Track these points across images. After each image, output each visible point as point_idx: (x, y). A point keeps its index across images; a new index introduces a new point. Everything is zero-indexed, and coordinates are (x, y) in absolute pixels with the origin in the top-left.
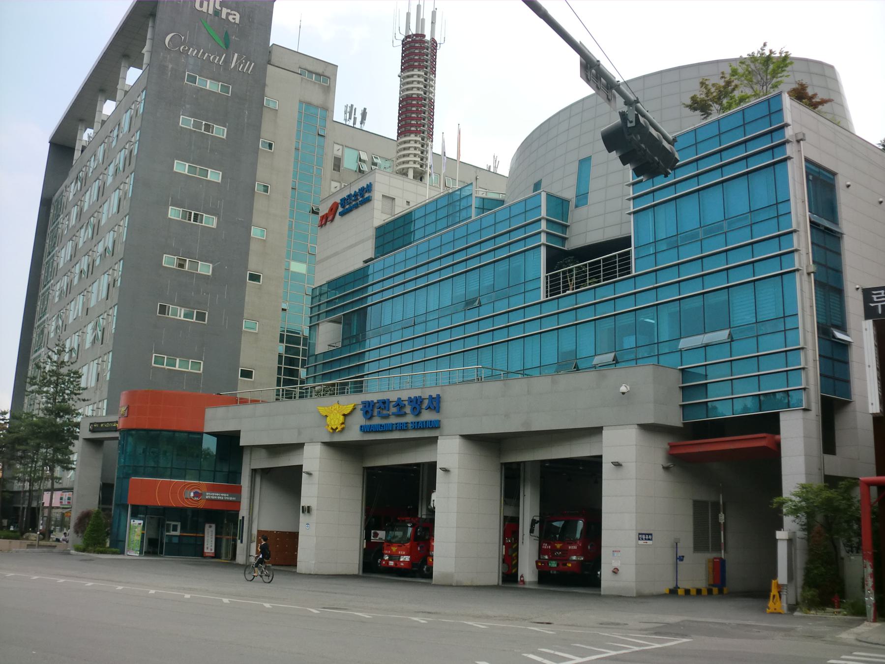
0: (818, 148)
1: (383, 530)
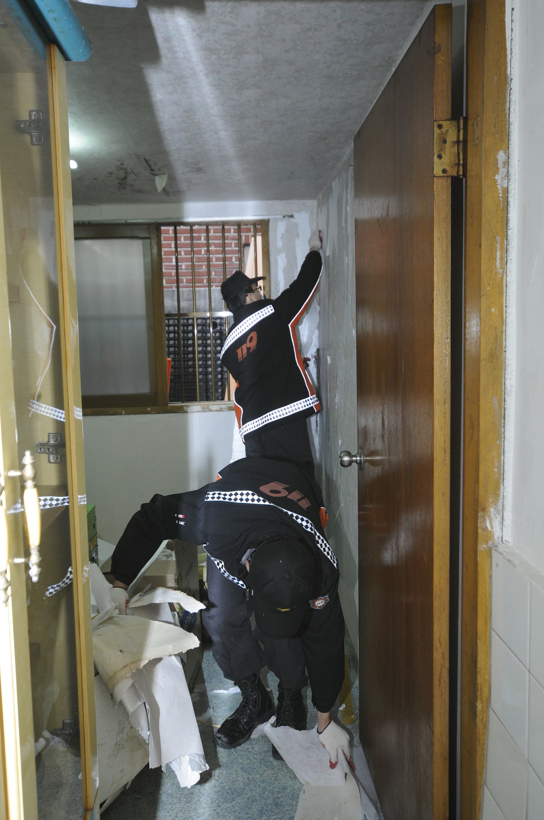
0: (241, 535)
1: (247, 454)
